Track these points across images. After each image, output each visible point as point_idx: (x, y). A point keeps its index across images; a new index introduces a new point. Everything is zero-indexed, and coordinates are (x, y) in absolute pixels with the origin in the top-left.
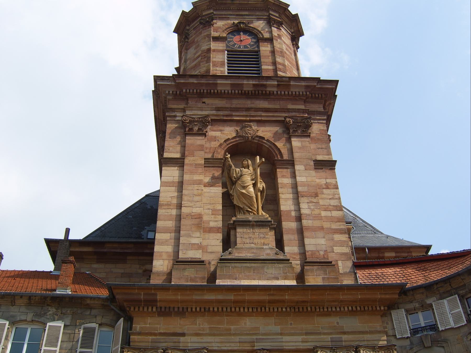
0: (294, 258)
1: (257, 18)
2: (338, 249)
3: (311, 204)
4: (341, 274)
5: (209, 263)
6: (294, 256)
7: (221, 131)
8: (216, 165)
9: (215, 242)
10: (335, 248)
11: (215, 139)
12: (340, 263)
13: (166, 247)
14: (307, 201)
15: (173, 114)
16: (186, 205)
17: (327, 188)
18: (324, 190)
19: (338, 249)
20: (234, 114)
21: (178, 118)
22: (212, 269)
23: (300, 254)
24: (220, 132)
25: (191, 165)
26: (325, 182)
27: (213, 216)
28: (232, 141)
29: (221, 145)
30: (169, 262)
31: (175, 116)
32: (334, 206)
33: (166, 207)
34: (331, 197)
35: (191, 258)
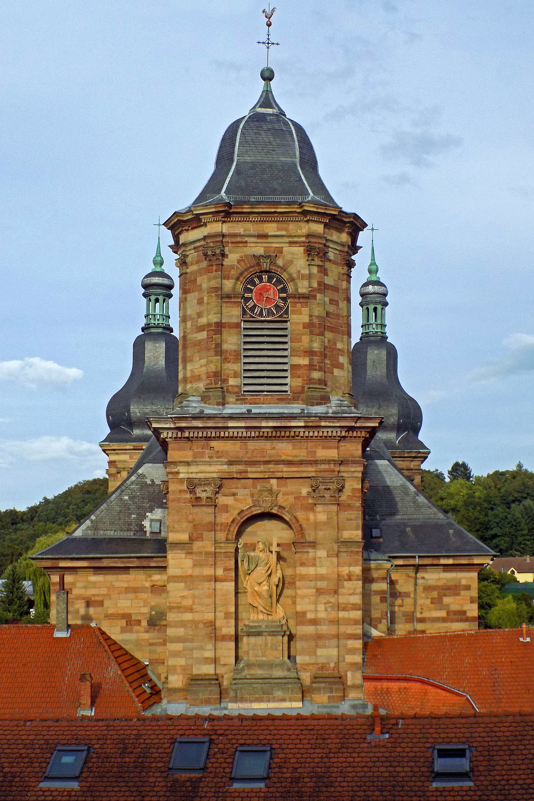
0: (305, 669)
1: (290, 243)
2: (349, 659)
3: (328, 605)
4: (349, 687)
5: (223, 677)
6: (305, 667)
7: (234, 495)
8: (276, 681)
9: (227, 651)
10: (346, 657)
11: (226, 508)
12: (349, 674)
13: (179, 659)
14: (324, 601)
15: (176, 470)
16: (197, 610)
17: (350, 579)
18: (345, 582)
19: (349, 659)
20: (249, 469)
21: (181, 476)
22: (158, 623)
23: (316, 575)
24: (232, 498)
25: (201, 553)
26: (347, 572)
27: (225, 621)
28: (246, 513)
29: (233, 521)
30: (184, 677)
31: (178, 473)
32: (353, 604)
33: (176, 610)
34: (351, 591)
35: (205, 675)
